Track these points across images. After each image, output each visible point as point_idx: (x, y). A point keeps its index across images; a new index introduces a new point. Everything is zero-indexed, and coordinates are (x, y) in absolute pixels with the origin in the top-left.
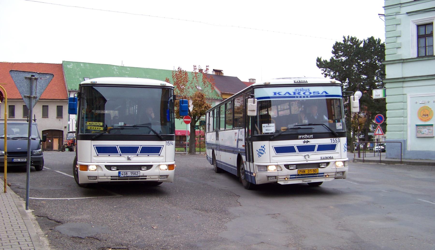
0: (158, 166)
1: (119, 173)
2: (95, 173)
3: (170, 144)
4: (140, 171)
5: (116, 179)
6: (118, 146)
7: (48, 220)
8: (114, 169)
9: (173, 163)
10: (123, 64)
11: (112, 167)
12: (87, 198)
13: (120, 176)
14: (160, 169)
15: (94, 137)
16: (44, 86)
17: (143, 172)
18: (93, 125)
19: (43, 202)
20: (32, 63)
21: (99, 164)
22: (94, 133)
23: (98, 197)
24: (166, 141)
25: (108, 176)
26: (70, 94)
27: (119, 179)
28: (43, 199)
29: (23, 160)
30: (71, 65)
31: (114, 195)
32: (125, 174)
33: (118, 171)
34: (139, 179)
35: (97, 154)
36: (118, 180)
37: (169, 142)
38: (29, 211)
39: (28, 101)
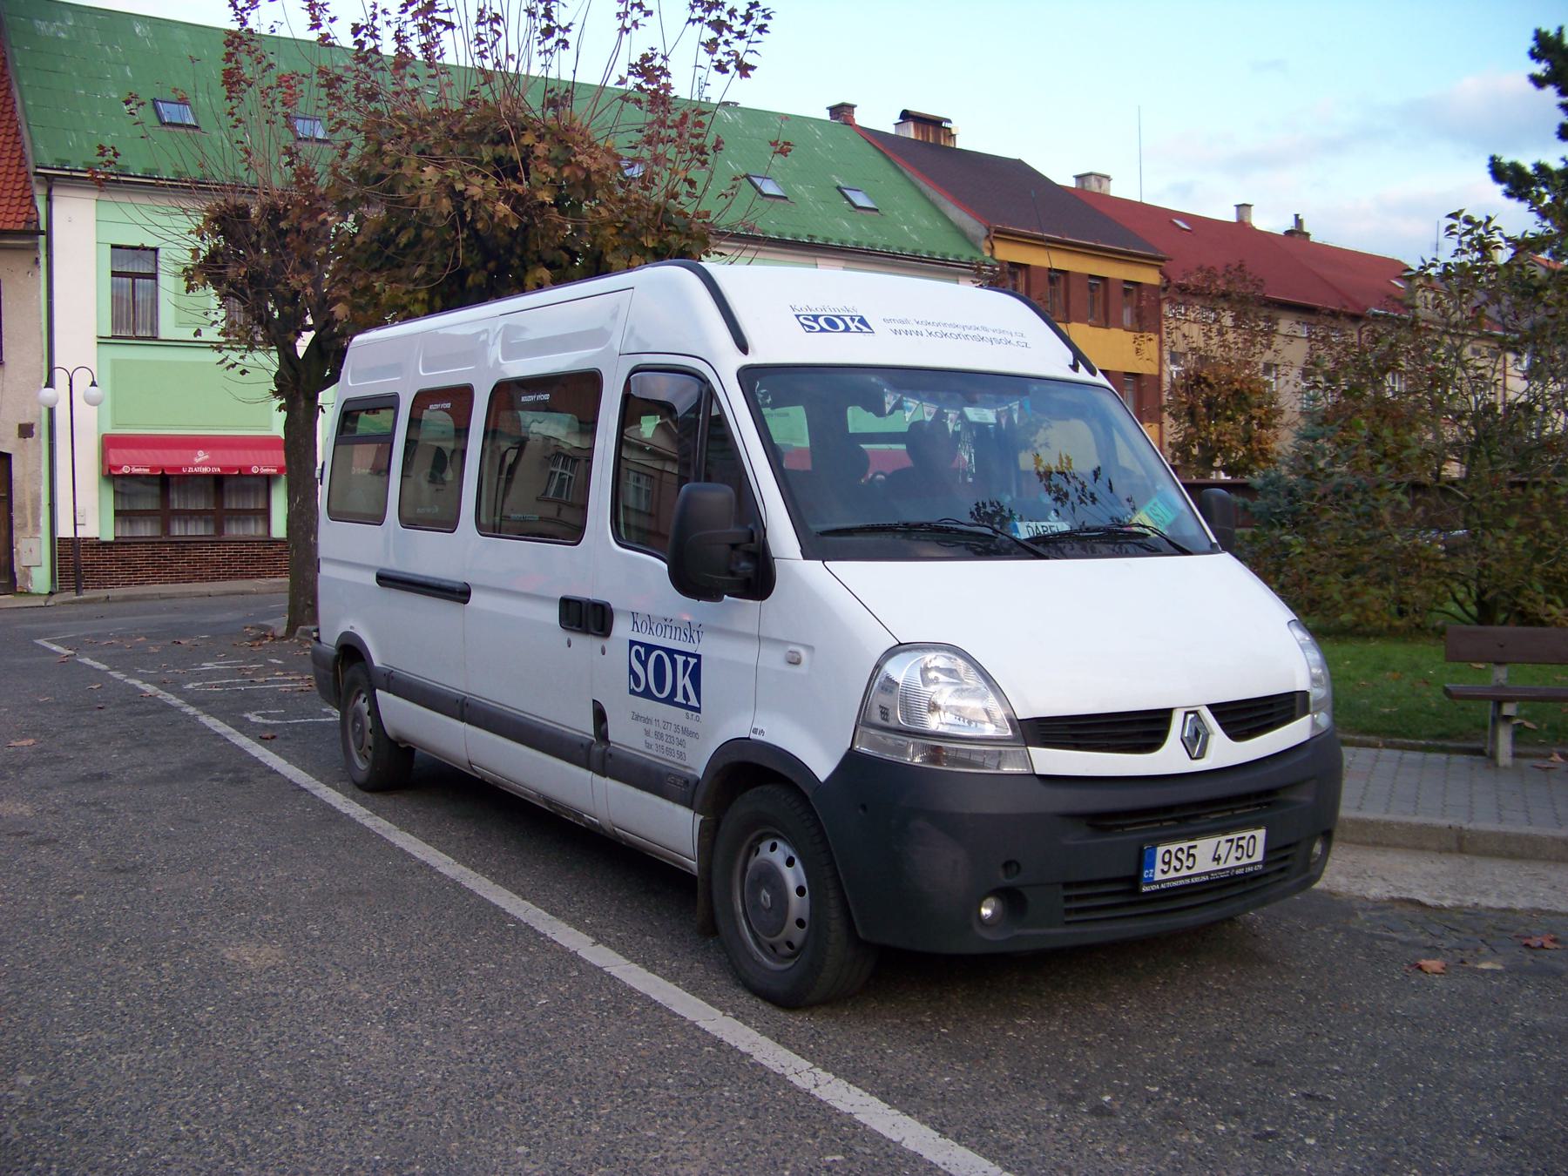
26: (49, 199)
30: (63, 21)
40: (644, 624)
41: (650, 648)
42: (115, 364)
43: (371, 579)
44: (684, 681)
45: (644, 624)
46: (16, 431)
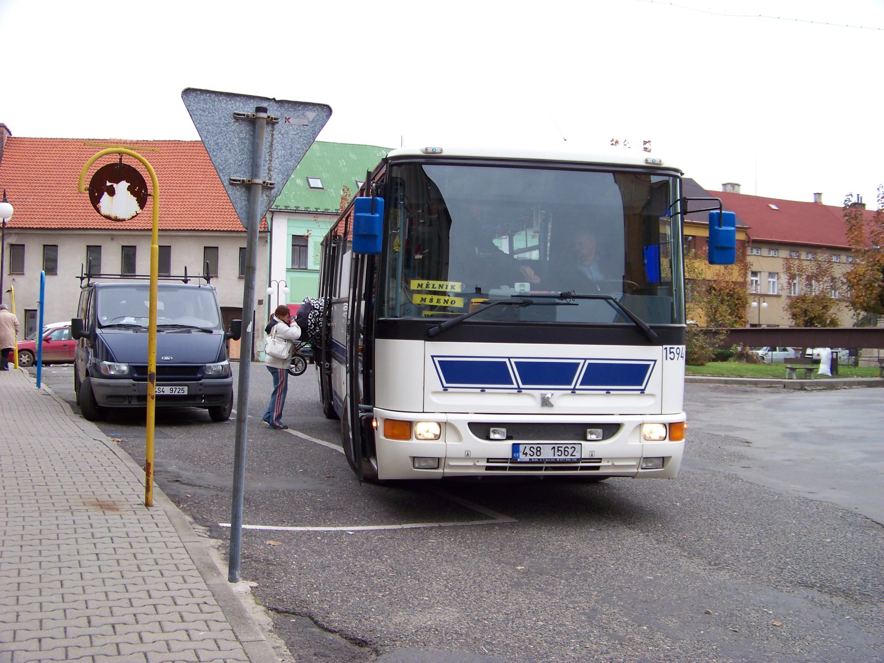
0: (638, 426)
1: (515, 448)
2: (435, 449)
3: (676, 356)
4: (581, 444)
5: (504, 468)
6: (513, 360)
7: (316, 630)
8: (497, 436)
9: (681, 417)
11: (492, 429)
12: (406, 526)
13: (519, 460)
14: (645, 439)
15: (433, 330)
16: (299, 146)
17: (591, 447)
18: (430, 289)
19: (272, 543)
20: (179, 141)
21: (451, 418)
22: (428, 316)
23: (443, 524)
24: (665, 346)
25: (478, 459)
26: (272, 219)
27: (511, 468)
28: (270, 531)
29: (178, 390)
31: (487, 517)
32: (535, 451)
33: (511, 442)
34: (575, 468)
35: (443, 387)
36: (507, 472)
37: (672, 350)
38: (242, 587)
39: (243, 198)
42: (292, 278)
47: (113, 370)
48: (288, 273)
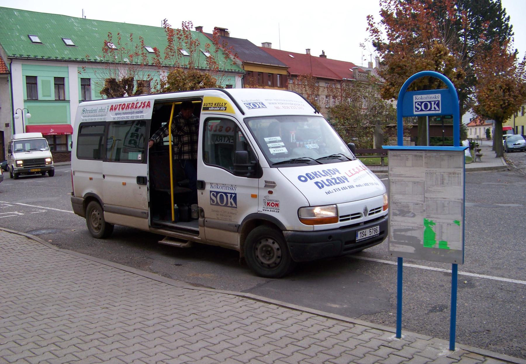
10: (85, 15)
26: (10, 65)
40: (215, 187)
41: (217, 193)
43: (135, 181)
44: (231, 200)
45: (215, 187)
46: (5, 125)
47: (473, 120)
48: (25, 103)
